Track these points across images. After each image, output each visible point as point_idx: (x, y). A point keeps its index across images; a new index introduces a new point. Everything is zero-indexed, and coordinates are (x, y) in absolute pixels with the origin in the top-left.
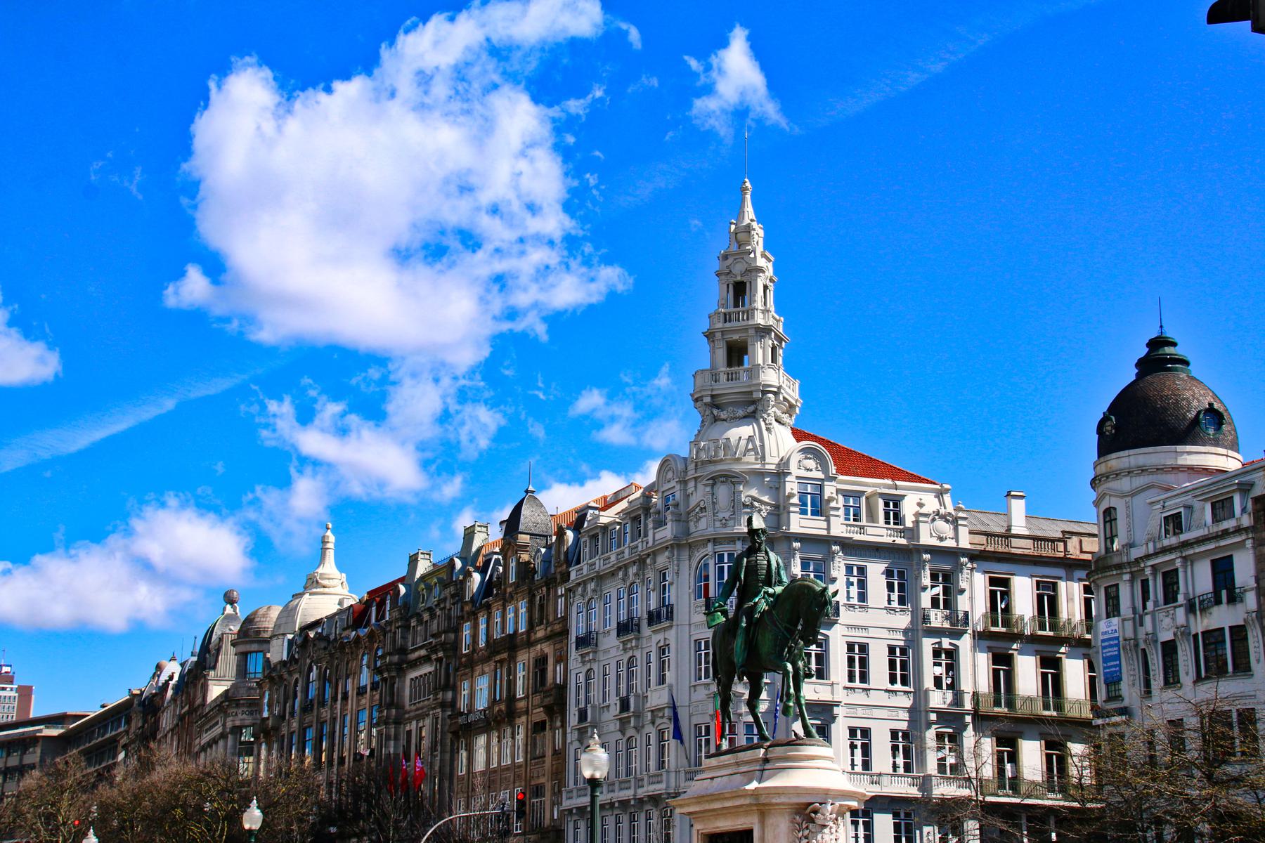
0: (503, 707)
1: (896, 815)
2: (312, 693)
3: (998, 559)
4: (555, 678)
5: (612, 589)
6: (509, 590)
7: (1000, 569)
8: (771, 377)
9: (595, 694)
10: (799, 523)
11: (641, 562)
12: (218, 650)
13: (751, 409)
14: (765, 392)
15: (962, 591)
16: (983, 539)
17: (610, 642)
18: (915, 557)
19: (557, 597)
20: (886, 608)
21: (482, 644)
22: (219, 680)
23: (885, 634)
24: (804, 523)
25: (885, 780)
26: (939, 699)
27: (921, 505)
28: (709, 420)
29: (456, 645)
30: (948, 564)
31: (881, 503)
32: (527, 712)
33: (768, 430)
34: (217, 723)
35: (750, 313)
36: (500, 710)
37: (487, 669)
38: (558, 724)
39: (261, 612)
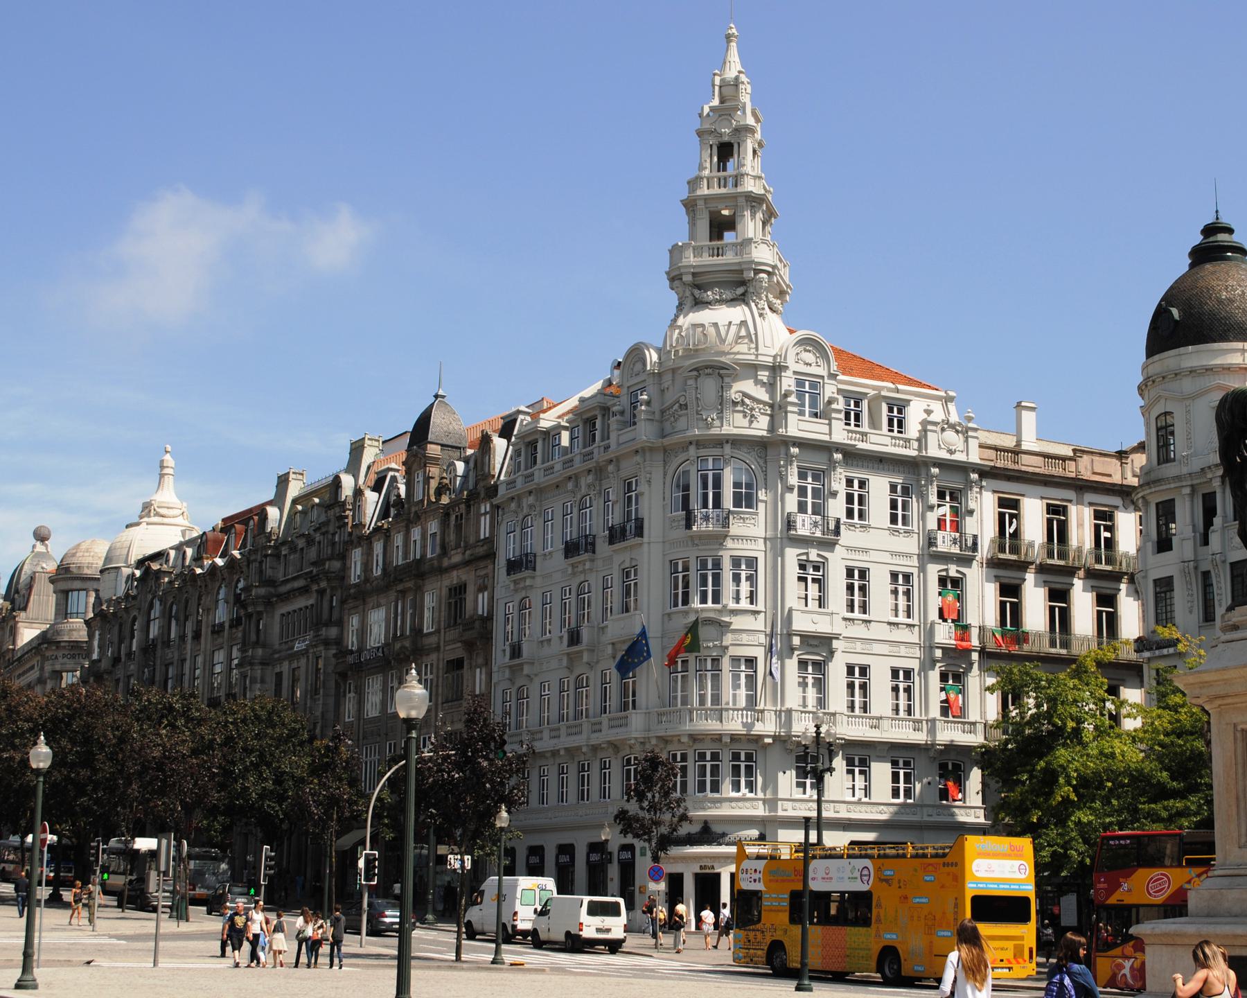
0: (407, 644)
1: (895, 764)
2: (154, 631)
3: (1007, 475)
4: (476, 608)
5: (555, 506)
6: (413, 509)
7: (1011, 489)
8: (763, 254)
9: (533, 628)
10: (797, 426)
11: (599, 472)
12: (30, 587)
13: (740, 290)
14: (757, 272)
15: (971, 513)
16: (991, 454)
17: (553, 564)
18: (923, 472)
19: (479, 515)
20: (889, 529)
21: (377, 572)
22: (31, 623)
23: (887, 558)
24: (803, 426)
25: (885, 724)
26: (944, 634)
27: (928, 412)
28: (689, 302)
29: (342, 575)
30: (956, 480)
31: (885, 407)
32: (438, 649)
33: (761, 315)
34: (32, 668)
35: (738, 179)
36: (403, 647)
37: (383, 601)
38: (480, 661)
39: (83, 547)
